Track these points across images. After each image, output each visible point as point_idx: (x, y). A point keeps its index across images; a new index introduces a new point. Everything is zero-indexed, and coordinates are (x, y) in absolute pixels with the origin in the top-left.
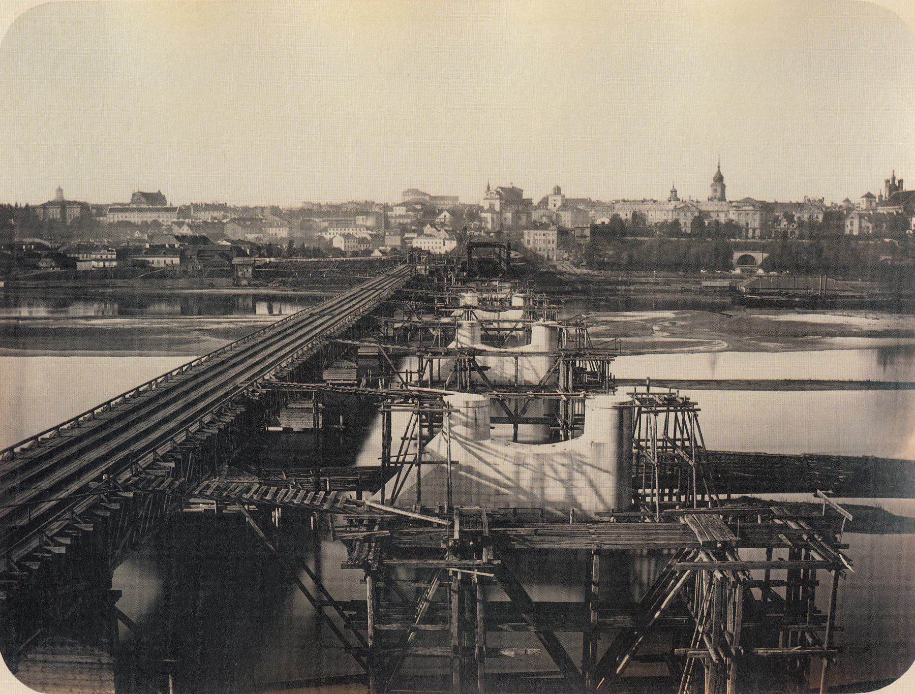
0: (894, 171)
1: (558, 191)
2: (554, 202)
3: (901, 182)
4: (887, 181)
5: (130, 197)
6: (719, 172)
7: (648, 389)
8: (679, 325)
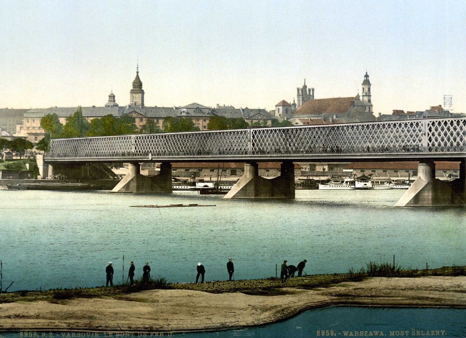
0: (305, 80)
6: (138, 77)
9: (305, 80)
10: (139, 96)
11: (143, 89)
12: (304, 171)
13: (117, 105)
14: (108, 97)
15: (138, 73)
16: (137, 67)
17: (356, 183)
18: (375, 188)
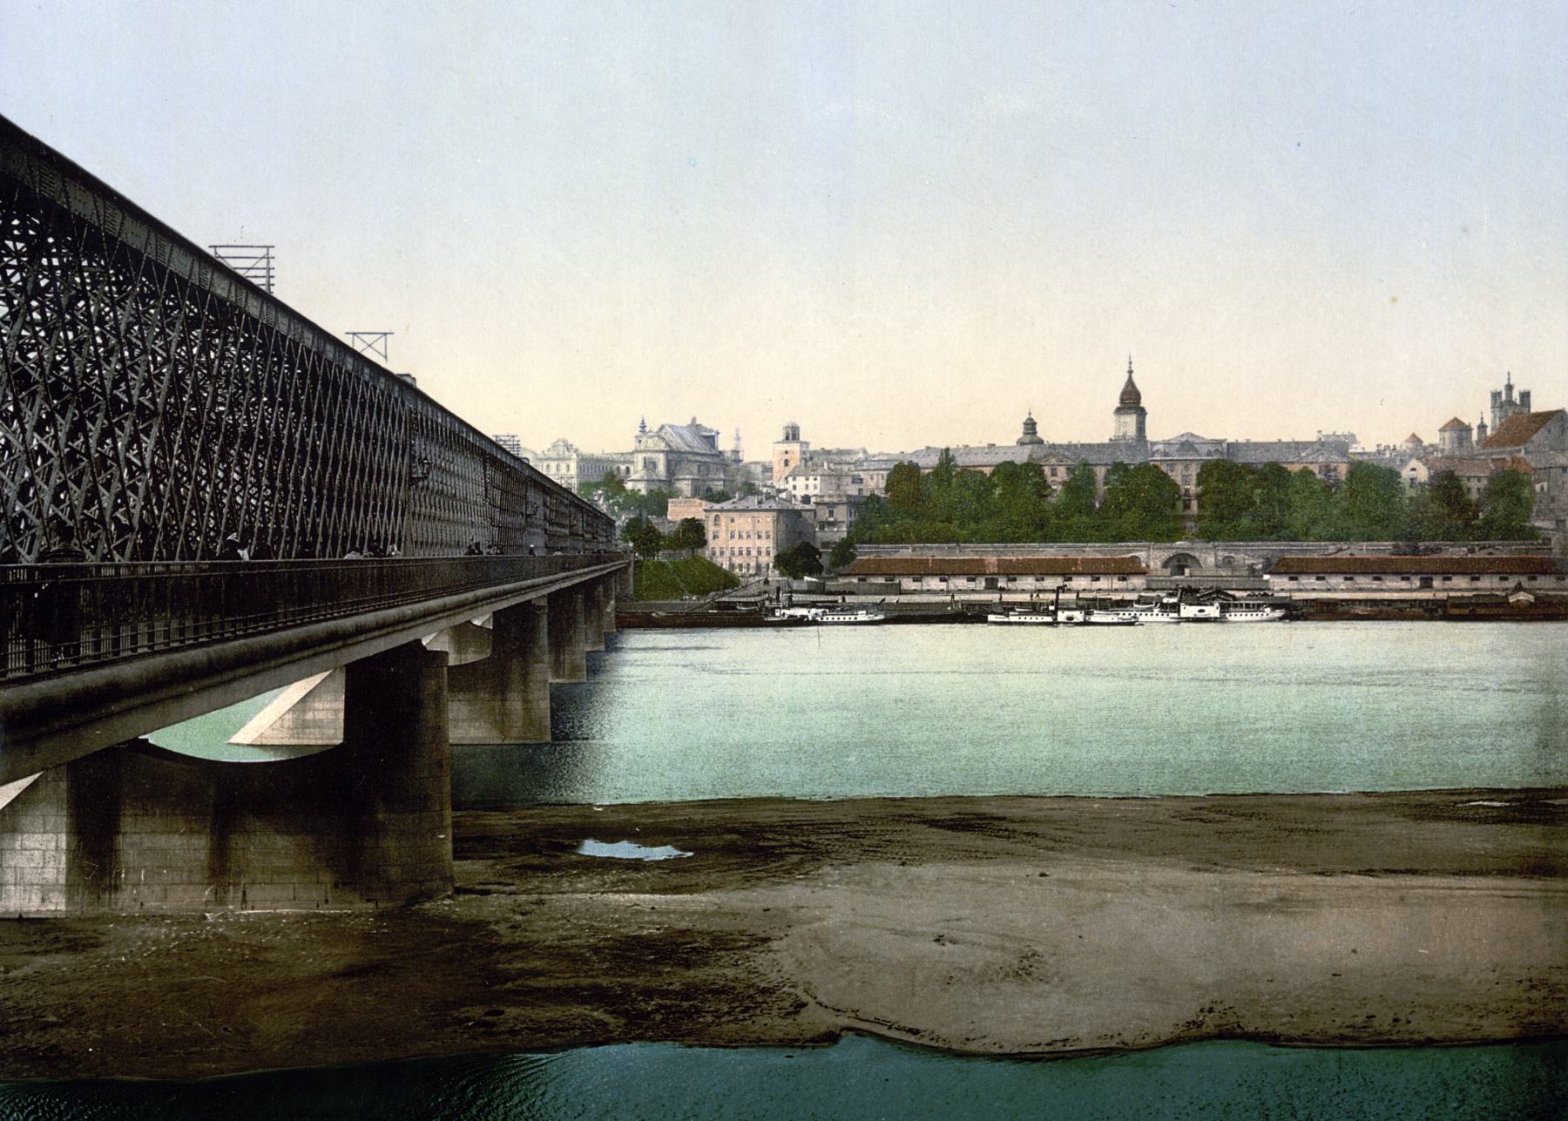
0: (1509, 374)
1: (792, 434)
2: (786, 457)
3: (1525, 396)
4: (1496, 395)
5: (805, 440)
6: (1130, 383)
7: (1078, 596)
8: (318, 520)
9: (1509, 374)
10: (1131, 420)
11: (1142, 405)
12: (220, 455)
13: (1041, 442)
14: (1438, 434)
15: (1130, 372)
16: (1128, 361)
17: (1182, 606)
18: (1230, 618)
